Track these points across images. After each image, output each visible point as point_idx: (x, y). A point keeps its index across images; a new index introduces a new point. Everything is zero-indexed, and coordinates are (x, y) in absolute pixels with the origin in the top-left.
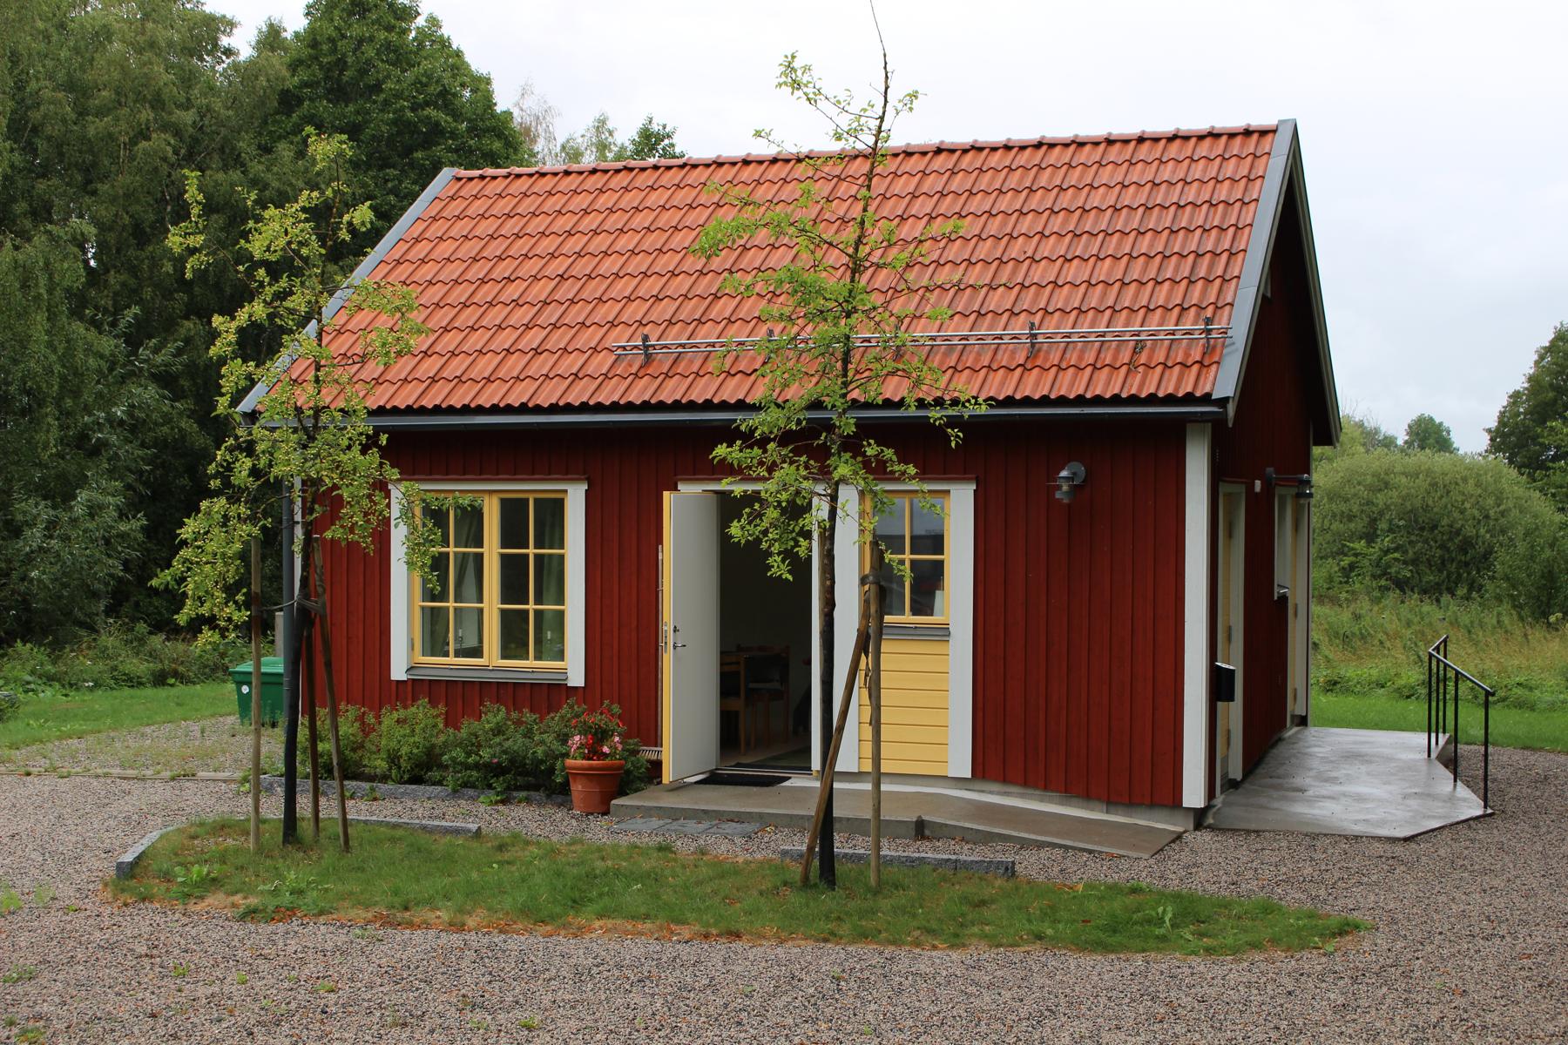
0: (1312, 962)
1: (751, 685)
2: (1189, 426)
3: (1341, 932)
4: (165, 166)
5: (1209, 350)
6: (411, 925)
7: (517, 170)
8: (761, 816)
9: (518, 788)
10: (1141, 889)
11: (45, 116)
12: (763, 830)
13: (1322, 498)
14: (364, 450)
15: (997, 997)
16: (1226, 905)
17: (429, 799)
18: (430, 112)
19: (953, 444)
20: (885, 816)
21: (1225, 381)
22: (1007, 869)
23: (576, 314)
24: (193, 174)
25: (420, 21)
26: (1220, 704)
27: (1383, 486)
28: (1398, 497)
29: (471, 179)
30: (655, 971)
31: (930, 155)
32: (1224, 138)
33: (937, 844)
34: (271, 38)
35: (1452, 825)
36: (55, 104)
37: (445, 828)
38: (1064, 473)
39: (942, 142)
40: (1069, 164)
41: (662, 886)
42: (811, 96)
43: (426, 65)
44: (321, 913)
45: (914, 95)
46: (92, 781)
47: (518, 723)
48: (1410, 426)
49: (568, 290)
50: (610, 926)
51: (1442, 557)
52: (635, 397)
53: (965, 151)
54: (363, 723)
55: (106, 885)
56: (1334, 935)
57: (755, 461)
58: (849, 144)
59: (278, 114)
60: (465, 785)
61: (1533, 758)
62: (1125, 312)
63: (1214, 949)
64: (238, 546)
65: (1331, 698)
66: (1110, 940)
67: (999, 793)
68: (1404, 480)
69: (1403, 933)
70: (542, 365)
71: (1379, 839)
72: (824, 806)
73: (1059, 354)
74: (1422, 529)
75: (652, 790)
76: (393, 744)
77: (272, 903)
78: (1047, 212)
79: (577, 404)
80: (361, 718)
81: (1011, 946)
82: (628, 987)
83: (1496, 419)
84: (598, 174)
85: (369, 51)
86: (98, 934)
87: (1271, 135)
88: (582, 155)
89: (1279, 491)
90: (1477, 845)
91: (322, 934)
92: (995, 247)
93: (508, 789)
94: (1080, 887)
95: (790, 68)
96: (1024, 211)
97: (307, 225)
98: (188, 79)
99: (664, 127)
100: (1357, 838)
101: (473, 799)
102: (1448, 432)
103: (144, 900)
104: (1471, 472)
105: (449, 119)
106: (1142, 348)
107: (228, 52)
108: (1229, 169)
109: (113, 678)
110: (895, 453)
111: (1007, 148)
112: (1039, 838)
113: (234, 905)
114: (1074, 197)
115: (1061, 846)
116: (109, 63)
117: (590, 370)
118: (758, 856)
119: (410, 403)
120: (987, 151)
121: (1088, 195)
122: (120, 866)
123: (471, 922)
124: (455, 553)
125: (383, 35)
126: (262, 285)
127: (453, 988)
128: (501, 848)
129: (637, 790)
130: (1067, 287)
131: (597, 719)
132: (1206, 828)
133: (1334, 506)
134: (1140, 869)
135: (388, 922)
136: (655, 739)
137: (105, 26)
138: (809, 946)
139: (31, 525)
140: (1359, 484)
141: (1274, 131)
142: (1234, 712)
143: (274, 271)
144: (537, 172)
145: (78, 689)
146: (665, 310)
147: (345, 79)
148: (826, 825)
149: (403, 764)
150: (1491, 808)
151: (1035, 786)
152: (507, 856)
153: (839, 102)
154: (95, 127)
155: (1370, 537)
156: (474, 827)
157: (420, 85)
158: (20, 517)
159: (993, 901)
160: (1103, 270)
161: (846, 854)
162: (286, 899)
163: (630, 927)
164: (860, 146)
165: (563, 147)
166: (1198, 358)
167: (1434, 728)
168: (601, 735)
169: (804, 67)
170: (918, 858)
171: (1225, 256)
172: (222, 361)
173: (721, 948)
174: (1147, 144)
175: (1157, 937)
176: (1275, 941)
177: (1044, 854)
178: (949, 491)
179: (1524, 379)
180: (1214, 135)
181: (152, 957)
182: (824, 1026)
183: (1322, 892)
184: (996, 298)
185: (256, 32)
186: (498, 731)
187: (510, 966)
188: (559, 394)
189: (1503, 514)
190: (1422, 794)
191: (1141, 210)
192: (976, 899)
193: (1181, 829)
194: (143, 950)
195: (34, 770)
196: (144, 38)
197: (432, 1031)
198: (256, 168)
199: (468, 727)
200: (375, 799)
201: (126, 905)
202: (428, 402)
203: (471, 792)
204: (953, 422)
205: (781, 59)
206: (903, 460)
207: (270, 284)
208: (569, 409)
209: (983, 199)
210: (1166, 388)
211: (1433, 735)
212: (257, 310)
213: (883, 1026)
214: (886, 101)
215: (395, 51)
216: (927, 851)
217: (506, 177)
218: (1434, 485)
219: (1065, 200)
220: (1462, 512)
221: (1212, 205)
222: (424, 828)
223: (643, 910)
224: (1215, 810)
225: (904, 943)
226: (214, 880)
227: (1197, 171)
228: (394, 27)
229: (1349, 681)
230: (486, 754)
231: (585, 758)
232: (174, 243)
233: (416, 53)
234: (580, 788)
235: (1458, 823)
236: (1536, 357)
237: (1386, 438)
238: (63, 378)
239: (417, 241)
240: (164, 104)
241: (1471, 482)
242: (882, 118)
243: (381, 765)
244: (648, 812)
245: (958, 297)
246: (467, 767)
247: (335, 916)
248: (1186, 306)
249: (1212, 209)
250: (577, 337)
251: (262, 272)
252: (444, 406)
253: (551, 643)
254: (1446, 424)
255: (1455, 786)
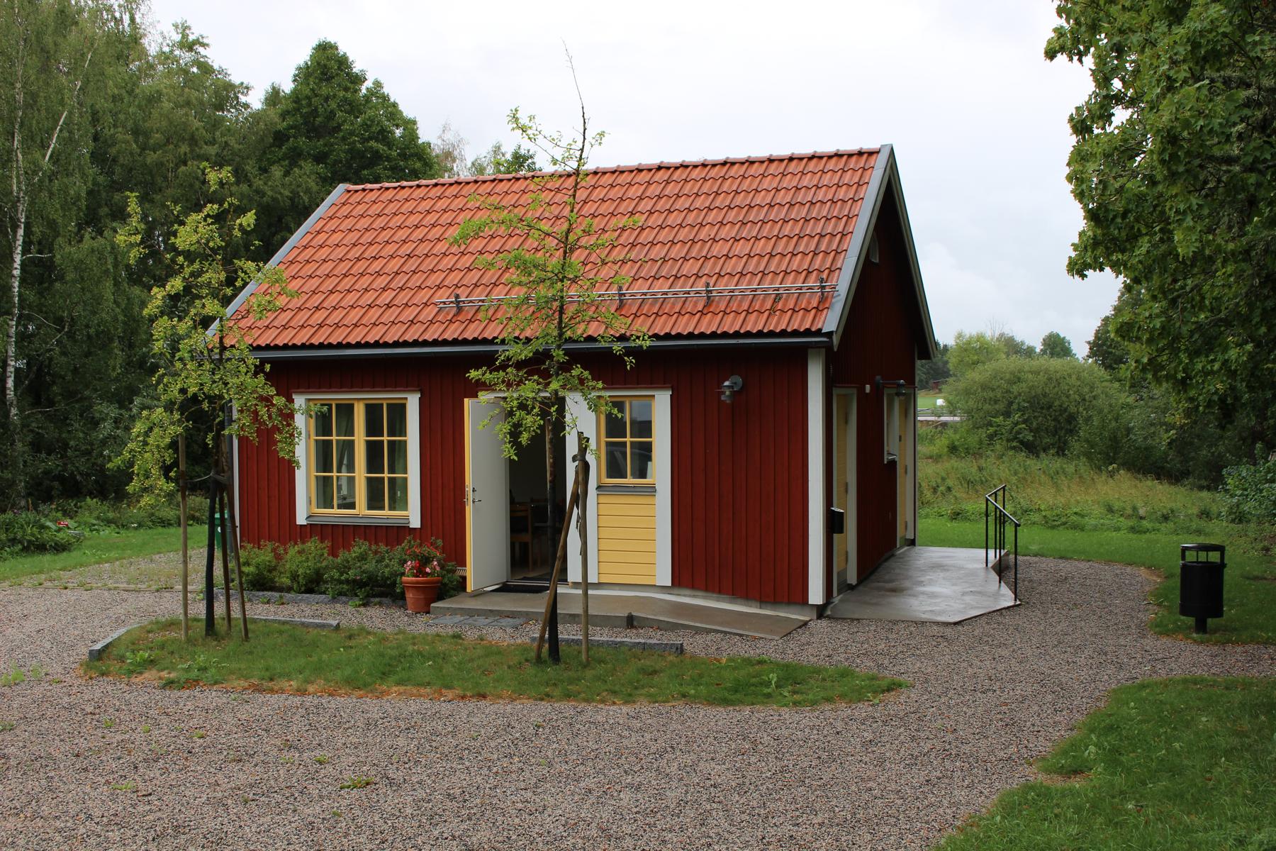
0: (862, 710)
1: (537, 525)
2: (810, 351)
3: (889, 690)
4: (197, 183)
5: (823, 299)
6: (272, 691)
7: (387, 185)
8: (527, 613)
9: (374, 596)
10: (765, 661)
11: (119, 152)
12: (527, 623)
13: (977, 389)
14: (256, 374)
15: (641, 738)
16: (818, 671)
17: (317, 603)
18: (373, 143)
19: (628, 367)
20: (590, 612)
21: (831, 321)
22: (677, 649)
23: (417, 280)
24: (134, 194)
25: (368, 84)
26: (836, 536)
27: (1016, 380)
28: (1027, 387)
29: (356, 191)
30: (419, 722)
31: (654, 171)
32: (845, 157)
33: (641, 631)
34: (274, 97)
35: (989, 613)
36: (124, 141)
37: (316, 624)
38: (727, 383)
39: (793, 154)
40: (743, 176)
41: (446, 663)
42: (531, 136)
43: (370, 113)
44: (216, 683)
45: (602, 134)
46: (105, 592)
47: (376, 553)
48: (1044, 340)
49: (412, 264)
50: (401, 691)
51: (1055, 426)
52: (448, 336)
53: (677, 168)
54: (276, 554)
55: (81, 665)
56: (883, 692)
57: (500, 380)
58: (559, 168)
59: (273, 146)
60: (341, 594)
61: (1063, 564)
62: (771, 275)
63: (800, 703)
64: (168, 440)
65: (955, 524)
66: (733, 697)
67: (690, 596)
68: (1030, 376)
69: (929, 689)
70: (390, 315)
71: (937, 623)
72: (550, 609)
73: (725, 304)
74: (1042, 408)
75: (461, 596)
76: (294, 567)
77: (183, 677)
78: (726, 208)
79: (470, 339)
80: (274, 550)
81: (664, 702)
82: (397, 733)
83: (1093, 335)
84: (439, 187)
85: (333, 105)
86: (66, 699)
87: (875, 155)
88: (485, 169)
89: (886, 391)
90: (1002, 627)
91: (213, 697)
92: (690, 232)
93: (368, 596)
94: (724, 661)
95: (515, 118)
96: (711, 208)
97: (214, 227)
98: (216, 124)
99: (529, 151)
100: (923, 623)
101: (345, 603)
102: (1069, 343)
103: (103, 675)
104: (1078, 371)
105: (385, 148)
106: (780, 299)
107: (246, 106)
108: (847, 178)
109: (152, 521)
110: (590, 374)
111: (704, 165)
112: (708, 626)
113: (160, 678)
114: (745, 198)
115: (722, 632)
116: (161, 115)
117: (421, 318)
118: (519, 641)
119: (304, 341)
120: (690, 168)
121: (754, 196)
122: (91, 652)
123: (311, 689)
124: (337, 441)
125: (342, 94)
126: (182, 266)
127: (283, 735)
128: (350, 637)
129: (451, 596)
130: (735, 258)
131: (426, 550)
132: (825, 617)
133: (985, 394)
134: (771, 648)
135: (258, 689)
136: (463, 563)
137: (158, 91)
138: (529, 703)
139: (104, 420)
140: (1001, 379)
141: (878, 152)
142: (849, 538)
143: (190, 256)
144: (514, 178)
145: (127, 529)
146: (473, 277)
147: (317, 123)
148: (552, 619)
149: (300, 579)
150: (1020, 600)
151: (713, 591)
152: (352, 643)
153: (553, 139)
154: (151, 157)
155: (1007, 414)
156: (334, 623)
157: (365, 126)
158: (97, 415)
159: (661, 671)
160: (759, 247)
161: (573, 640)
162: (194, 674)
163: (415, 691)
164: (568, 169)
165: (473, 164)
166: (815, 305)
167: (998, 546)
168: (426, 560)
169: (530, 117)
170: (620, 642)
171: (839, 236)
172: (152, 320)
173: (471, 705)
174: (795, 161)
175: (765, 694)
176: (842, 696)
177: (709, 637)
178: (654, 396)
179: (1111, 308)
180: (838, 155)
181: (94, 714)
182: (516, 759)
183: (886, 662)
184: (688, 266)
185: (264, 93)
186: (363, 558)
187: (324, 720)
188: (399, 334)
189: (1094, 398)
190: (980, 593)
191: (787, 206)
192: (651, 669)
193: (807, 619)
194: (89, 709)
195: (70, 585)
196: (183, 99)
197: (256, 765)
198: (258, 183)
199: (343, 555)
200: (283, 604)
201: (91, 678)
202: (315, 341)
203: (344, 598)
204: (629, 352)
205: (509, 112)
206: (596, 378)
207: (188, 266)
208: (406, 344)
209: (685, 200)
210: (793, 326)
211: (998, 551)
212: (176, 284)
213: (556, 759)
214: (584, 139)
215: (350, 104)
216: (631, 637)
217: (379, 190)
218: (1050, 379)
219: (739, 200)
220: (1068, 397)
221: (833, 202)
222: (303, 624)
223: (427, 680)
224: (832, 605)
225: (593, 700)
226: (152, 661)
227: (826, 179)
228: (349, 88)
229: (967, 512)
230: (351, 574)
231: (414, 576)
232: (120, 241)
233: (364, 105)
234: (411, 595)
235: (994, 611)
236: (1119, 294)
237: (1028, 347)
238: (125, 323)
239: (319, 233)
240: (196, 142)
241: (1074, 377)
242: (582, 150)
243: (285, 581)
244: (454, 612)
245: (663, 266)
246: (340, 582)
247: (224, 686)
248: (810, 270)
249: (834, 205)
250: (415, 297)
251: (181, 258)
252: (325, 343)
253: (399, 501)
254: (1067, 338)
255: (1000, 586)
